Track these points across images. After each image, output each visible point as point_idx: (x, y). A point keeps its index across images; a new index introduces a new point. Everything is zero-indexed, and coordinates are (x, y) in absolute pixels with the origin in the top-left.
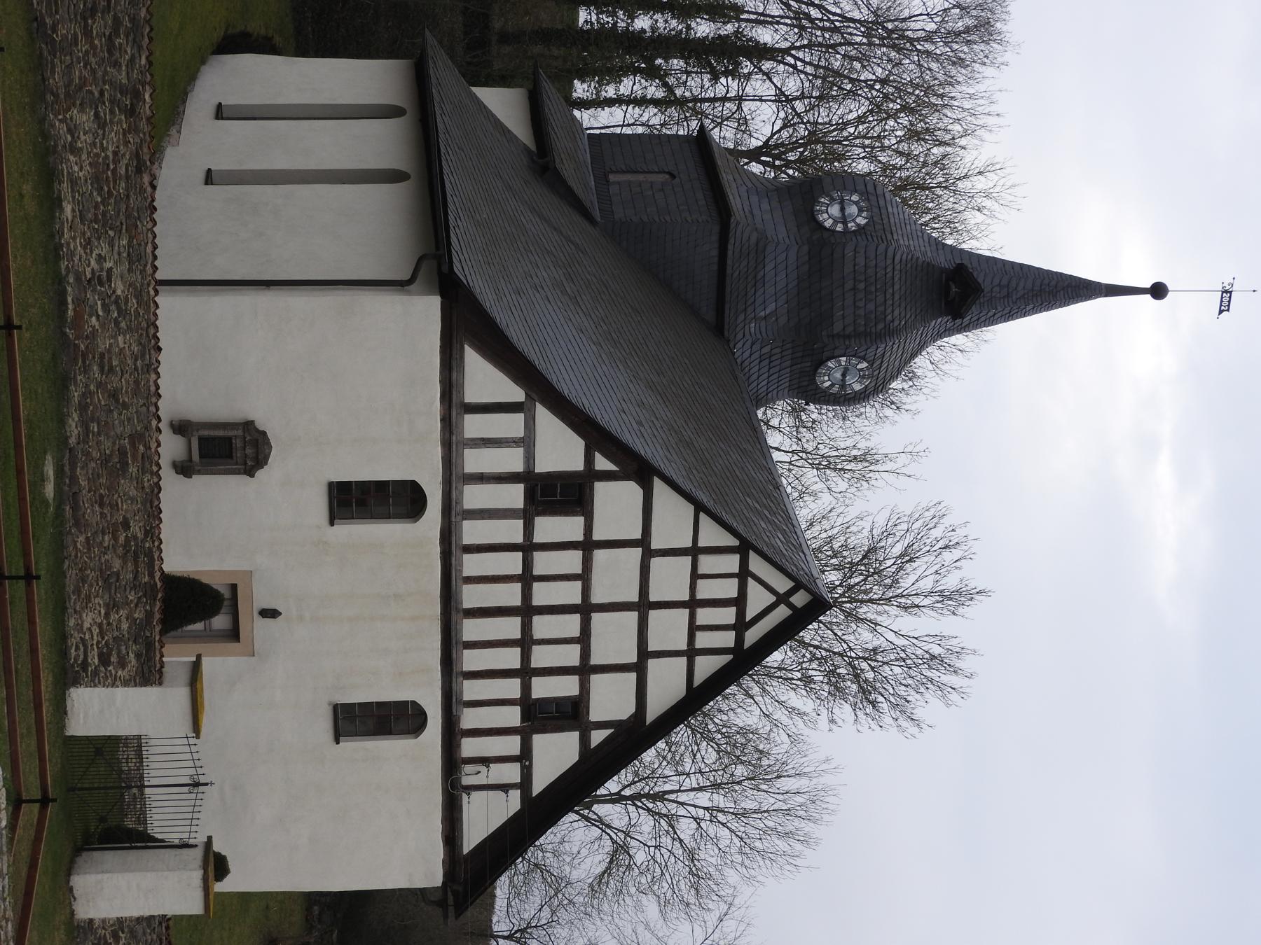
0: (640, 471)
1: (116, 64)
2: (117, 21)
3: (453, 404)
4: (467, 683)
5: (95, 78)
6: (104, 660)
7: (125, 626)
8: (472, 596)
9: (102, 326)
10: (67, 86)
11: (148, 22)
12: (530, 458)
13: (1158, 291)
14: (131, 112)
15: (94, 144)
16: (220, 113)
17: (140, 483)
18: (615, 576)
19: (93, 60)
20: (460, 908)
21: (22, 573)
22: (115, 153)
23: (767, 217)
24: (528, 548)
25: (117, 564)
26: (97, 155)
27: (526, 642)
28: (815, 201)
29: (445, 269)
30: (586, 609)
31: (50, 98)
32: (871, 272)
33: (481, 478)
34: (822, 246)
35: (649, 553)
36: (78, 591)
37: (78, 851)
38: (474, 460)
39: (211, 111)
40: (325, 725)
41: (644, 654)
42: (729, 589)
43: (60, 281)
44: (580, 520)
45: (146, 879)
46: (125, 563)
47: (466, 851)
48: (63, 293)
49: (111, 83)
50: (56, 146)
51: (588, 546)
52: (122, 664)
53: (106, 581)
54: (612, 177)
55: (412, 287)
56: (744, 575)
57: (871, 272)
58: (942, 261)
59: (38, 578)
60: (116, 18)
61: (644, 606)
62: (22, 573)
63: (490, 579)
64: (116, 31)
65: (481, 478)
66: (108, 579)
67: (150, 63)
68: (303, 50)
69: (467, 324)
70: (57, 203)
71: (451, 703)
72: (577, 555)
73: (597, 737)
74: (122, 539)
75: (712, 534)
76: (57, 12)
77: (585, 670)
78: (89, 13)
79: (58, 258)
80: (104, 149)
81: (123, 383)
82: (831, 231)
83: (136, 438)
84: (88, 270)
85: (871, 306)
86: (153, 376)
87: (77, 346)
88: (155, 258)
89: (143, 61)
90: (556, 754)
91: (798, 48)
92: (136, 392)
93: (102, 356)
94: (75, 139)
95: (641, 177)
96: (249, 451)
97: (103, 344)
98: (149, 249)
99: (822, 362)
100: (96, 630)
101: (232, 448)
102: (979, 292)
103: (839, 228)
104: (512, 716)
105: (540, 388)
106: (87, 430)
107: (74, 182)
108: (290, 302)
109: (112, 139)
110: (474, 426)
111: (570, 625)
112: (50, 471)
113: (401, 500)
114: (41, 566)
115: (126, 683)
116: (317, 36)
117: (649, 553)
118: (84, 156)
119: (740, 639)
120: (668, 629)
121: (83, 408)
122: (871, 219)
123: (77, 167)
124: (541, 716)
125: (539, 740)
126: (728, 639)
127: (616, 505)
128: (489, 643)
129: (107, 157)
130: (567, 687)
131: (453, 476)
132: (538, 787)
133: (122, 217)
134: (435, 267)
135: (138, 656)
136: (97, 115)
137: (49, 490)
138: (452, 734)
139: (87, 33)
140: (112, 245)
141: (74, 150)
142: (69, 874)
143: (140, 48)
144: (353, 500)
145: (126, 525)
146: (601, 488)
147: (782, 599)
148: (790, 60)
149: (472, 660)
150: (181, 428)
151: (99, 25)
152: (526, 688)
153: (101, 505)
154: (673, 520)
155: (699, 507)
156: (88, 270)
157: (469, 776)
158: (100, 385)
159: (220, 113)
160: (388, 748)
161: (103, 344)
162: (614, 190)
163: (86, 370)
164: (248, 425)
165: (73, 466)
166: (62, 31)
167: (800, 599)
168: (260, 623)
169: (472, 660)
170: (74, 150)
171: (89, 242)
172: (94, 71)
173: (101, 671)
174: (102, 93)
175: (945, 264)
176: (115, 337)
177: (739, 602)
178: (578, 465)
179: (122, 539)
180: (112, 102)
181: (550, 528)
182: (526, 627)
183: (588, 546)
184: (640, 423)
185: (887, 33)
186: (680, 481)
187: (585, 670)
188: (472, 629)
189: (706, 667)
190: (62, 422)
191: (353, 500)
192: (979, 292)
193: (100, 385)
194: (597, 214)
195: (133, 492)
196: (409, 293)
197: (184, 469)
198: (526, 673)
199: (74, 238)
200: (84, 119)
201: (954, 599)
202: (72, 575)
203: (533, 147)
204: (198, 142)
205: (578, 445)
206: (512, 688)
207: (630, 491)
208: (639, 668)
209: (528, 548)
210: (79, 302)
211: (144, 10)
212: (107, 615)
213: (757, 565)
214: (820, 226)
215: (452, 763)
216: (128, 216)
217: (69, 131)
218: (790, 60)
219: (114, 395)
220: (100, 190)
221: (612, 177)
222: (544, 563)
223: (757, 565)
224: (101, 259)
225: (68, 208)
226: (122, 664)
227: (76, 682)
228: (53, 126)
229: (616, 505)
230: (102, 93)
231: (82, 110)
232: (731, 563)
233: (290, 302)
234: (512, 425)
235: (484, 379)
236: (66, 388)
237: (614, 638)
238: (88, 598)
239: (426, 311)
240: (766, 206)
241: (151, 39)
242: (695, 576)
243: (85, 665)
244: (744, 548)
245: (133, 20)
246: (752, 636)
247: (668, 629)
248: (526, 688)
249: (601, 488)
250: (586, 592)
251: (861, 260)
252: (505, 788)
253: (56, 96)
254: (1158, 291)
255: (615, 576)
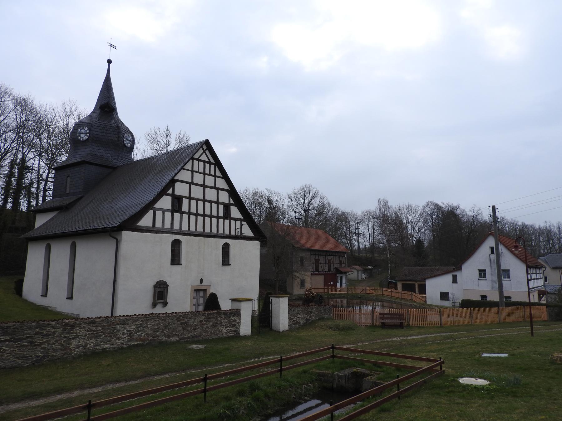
0: (173, 182)
1: (54, 333)
2: (37, 333)
3: (152, 230)
4: (219, 232)
5: (59, 340)
6: (234, 326)
7: (226, 320)
8: (200, 229)
9: (145, 332)
10: (61, 350)
11: (38, 322)
12: (168, 210)
13: (109, 62)
14: (73, 326)
15: (84, 339)
16: (45, 295)
17: (190, 318)
18: (197, 192)
19: (52, 341)
20: (265, 238)
21: (280, 363)
22: (88, 331)
23: (83, 153)
24: (190, 214)
25: (211, 324)
26: (88, 337)
27: (211, 217)
28: (79, 140)
29: (116, 229)
30: (204, 201)
31: (65, 356)
32: (101, 128)
33: (172, 224)
34: (93, 140)
35: (190, 184)
36: (217, 334)
37: (271, 329)
38: (168, 225)
39: (43, 298)
40: (227, 268)
41: (215, 188)
42: (201, 164)
43: (130, 347)
44: (184, 199)
45: (281, 311)
46: (211, 321)
47: (253, 235)
48: (134, 345)
49: (61, 334)
50: (83, 352)
51: (190, 198)
52: (235, 321)
53: (215, 326)
54: (68, 192)
55: (119, 239)
56: (198, 160)
57: (101, 128)
58: (98, 112)
59: (281, 357)
60: (36, 334)
61: (204, 186)
62: (280, 363)
63: (196, 224)
64: (41, 334)
65: (172, 224)
66: (215, 326)
67: (54, 320)
68: (23, 273)
69: (131, 224)
70: (104, 350)
71: (223, 237)
72: (192, 201)
73: (232, 202)
74: (205, 322)
75: (188, 166)
76: (31, 356)
77: (218, 203)
78: (33, 344)
79: (122, 348)
80: (86, 335)
81: (162, 324)
82: (89, 137)
83: (178, 320)
84: (127, 338)
85: (111, 130)
86: (161, 315)
87: (151, 340)
88: (124, 316)
89: (54, 323)
90: (235, 212)
91: (23, 151)
92: (165, 320)
93: (154, 331)
94: (81, 346)
95: (68, 185)
96: (162, 286)
97: (150, 331)
98: (121, 318)
99: (124, 145)
100: (227, 329)
101: (161, 291)
102: (106, 104)
103: (88, 135)
104: (227, 221)
105: (150, 206)
106: (175, 335)
107: (97, 345)
108: (65, 280)
109: (83, 332)
110: (158, 225)
111: (208, 205)
112: (194, 346)
113: (176, 244)
114: (277, 357)
115: (240, 319)
116: (18, 269)
117: (190, 184)
118: (88, 342)
119: (213, 164)
120: (210, 181)
121: (169, 336)
122: (86, 127)
123: (92, 344)
124: (227, 215)
125: (232, 216)
126: (213, 166)
127: (180, 189)
128: (211, 226)
129: (89, 334)
130: (221, 207)
131: (171, 232)
132: (241, 217)
133: (110, 328)
134: (112, 233)
135: (233, 316)
136: (73, 339)
137: (201, 346)
138: (230, 237)
139: (41, 344)
140: (119, 331)
141: (86, 345)
142: (279, 332)
143: (48, 324)
144: (175, 259)
145: (201, 321)
146: (176, 193)
147: (204, 152)
148: (26, 153)
149: (214, 231)
150: (154, 305)
151: (38, 340)
152: (221, 218)
153: (196, 329)
154: (185, 175)
155: (182, 168)
156: (127, 338)
157: (238, 233)
158: (162, 332)
159: (45, 295)
160: (232, 251)
161: (150, 331)
162: (72, 191)
163: (158, 336)
164: (155, 286)
165: (185, 338)
166: (39, 354)
167: (205, 147)
168: (204, 284)
169: (214, 231)
170: (86, 345)
171: (118, 338)
172: (56, 341)
173: (236, 326)
174: (65, 337)
175: (99, 111)
176: (148, 328)
177: (205, 162)
178: (170, 198)
179: (205, 322)
180: (69, 334)
181: (185, 208)
182: (208, 216)
183: (190, 198)
184: (157, 182)
185: (21, 128)
186: (176, 172)
187: (218, 203)
188: (207, 230)
189: (218, 173)
190: (173, 343)
191: (175, 259)
192: (106, 104)
193: (162, 332)
194: (80, 196)
195: (193, 320)
196: (121, 240)
197: (165, 304)
198: (218, 217)
199: (116, 343)
200: (74, 343)
201: (168, 134)
202: (214, 337)
203: (58, 212)
204: (56, 300)
205: (165, 197)
206: (221, 221)
207: (177, 185)
208: (218, 189)
209: (190, 214)
210: (137, 340)
211: (33, 324)
212: (223, 326)
213: (196, 156)
214: (87, 140)
215: (236, 237)
216: (110, 325)
217: (78, 348)
218: (26, 153)
219: (166, 327)
220: (100, 336)
221: (68, 192)
222: (193, 210)
223: (196, 156)
224: (123, 334)
225: (106, 346)
226: (235, 321)
227: (239, 333)
228: (76, 354)
229: (180, 189)
230: (65, 337)
231: (71, 344)
232: (196, 162)
233: (65, 280)
234: (159, 214)
235: (146, 221)
236: (163, 342)
237: (211, 195)
238: (219, 331)
239: (126, 235)
240: (80, 153)
241: (45, 321)
242: (198, 172)
243: (235, 331)
244: (193, 159)
245: (37, 328)
246: (212, 161)
247: (210, 181)
248: (221, 218)
249: (176, 193)
250: (200, 200)
251: (98, 130)
252: (241, 225)
253: (65, 354)
254: (109, 62)
255: (197, 192)
